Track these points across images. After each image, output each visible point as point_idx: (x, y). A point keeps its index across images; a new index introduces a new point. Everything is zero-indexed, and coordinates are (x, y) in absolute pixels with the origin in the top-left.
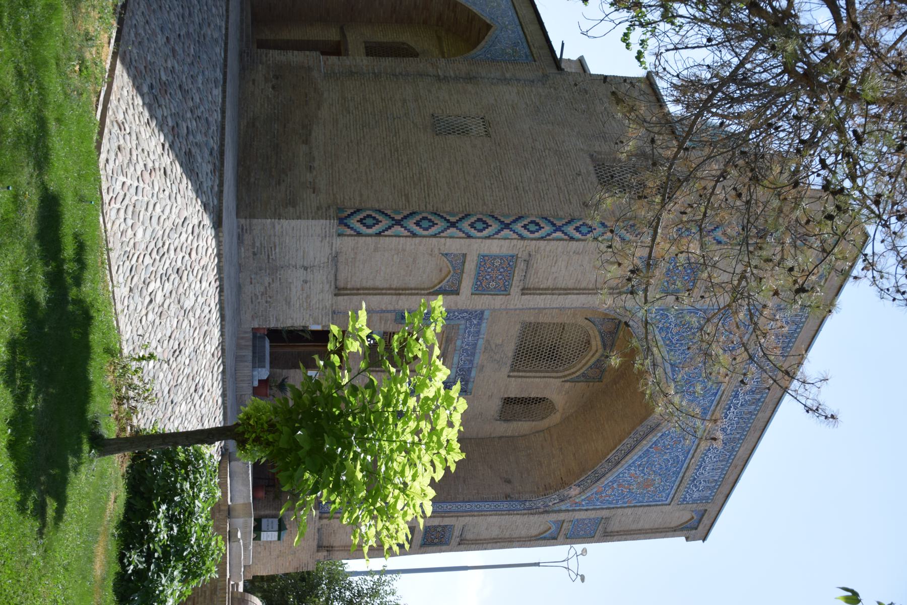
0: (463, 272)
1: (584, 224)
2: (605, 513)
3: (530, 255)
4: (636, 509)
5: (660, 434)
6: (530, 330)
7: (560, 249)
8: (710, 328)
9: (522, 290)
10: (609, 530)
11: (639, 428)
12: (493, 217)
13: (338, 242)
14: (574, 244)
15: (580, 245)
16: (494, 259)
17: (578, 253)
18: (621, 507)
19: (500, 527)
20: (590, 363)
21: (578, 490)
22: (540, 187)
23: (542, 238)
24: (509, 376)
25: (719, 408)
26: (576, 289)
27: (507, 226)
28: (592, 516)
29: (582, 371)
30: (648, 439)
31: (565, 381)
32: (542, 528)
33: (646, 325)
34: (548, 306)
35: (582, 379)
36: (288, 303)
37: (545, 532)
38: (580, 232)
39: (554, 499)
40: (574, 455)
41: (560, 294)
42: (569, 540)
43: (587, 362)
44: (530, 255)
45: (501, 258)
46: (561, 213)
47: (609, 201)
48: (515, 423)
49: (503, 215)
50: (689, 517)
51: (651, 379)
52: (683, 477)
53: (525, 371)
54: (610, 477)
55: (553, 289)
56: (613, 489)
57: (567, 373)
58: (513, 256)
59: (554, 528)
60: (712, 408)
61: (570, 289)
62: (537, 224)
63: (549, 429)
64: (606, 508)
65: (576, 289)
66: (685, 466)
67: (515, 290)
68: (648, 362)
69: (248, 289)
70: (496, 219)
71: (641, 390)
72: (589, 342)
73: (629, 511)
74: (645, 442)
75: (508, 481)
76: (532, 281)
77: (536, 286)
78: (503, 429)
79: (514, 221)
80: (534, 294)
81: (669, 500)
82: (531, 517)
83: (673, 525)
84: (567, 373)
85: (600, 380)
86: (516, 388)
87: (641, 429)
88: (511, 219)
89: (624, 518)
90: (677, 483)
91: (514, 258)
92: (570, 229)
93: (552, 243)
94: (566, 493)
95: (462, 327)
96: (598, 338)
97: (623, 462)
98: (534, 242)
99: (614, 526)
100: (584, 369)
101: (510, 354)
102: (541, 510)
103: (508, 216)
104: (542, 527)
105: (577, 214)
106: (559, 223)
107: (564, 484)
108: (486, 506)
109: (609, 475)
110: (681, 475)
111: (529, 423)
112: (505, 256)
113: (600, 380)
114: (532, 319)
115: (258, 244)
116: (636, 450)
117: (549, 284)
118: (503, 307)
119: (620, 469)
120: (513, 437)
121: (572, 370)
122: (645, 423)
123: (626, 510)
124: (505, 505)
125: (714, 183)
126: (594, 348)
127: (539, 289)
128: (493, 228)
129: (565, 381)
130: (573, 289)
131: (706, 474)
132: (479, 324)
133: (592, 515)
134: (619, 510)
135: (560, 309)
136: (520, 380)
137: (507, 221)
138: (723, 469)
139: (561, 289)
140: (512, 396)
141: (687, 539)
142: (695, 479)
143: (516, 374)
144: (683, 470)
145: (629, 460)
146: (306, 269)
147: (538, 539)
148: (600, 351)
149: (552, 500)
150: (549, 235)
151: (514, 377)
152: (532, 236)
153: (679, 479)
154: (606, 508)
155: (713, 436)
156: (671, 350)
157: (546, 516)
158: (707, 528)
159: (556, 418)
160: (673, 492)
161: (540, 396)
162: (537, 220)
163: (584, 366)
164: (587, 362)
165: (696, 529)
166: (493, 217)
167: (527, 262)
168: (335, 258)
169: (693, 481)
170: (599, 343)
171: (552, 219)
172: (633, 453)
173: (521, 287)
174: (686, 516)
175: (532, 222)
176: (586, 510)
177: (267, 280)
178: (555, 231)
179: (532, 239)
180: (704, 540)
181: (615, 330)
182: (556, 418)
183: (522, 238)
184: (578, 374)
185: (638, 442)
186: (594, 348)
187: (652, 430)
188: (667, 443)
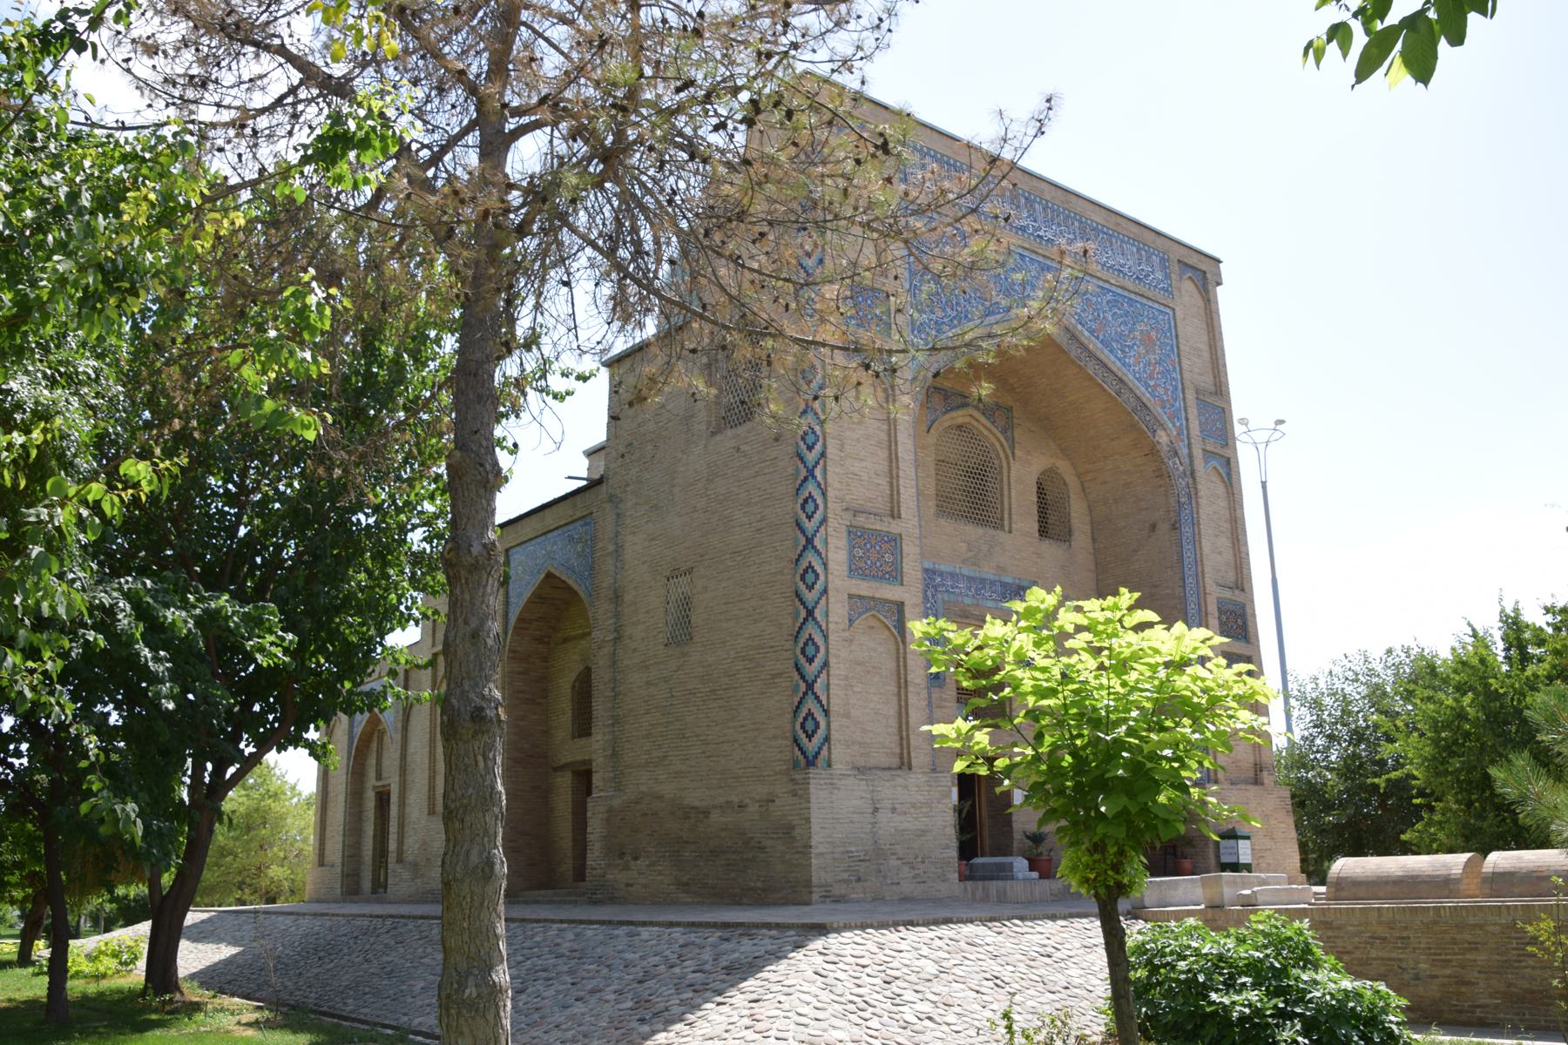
0: (873, 598)
13: (839, 767)
36: (924, 832)
69: (908, 888)
95: (946, 597)
108: (1188, 556)
115: (845, 876)
124: (1187, 530)
132: (941, 574)
146: (876, 810)
159: (1064, 468)
168: (861, 770)
177: (893, 862)
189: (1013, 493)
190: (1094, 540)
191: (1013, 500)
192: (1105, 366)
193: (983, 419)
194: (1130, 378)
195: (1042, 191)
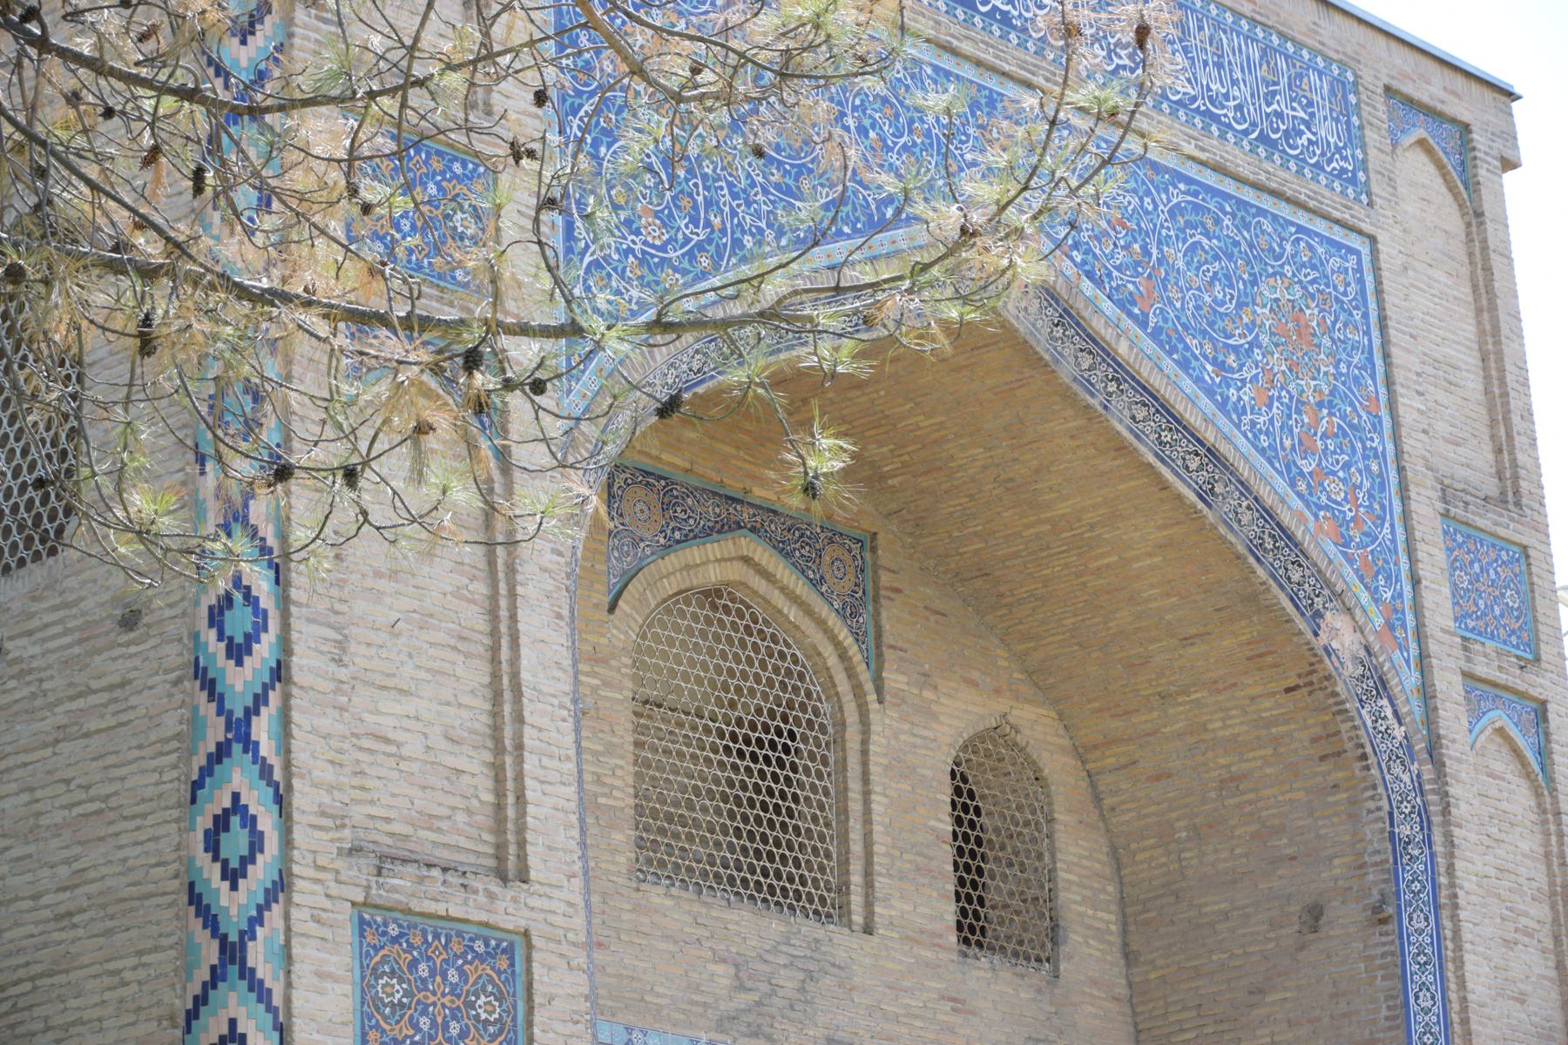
1: (216, 617)
2: (1425, 507)
3: (355, 851)
4: (1399, 375)
5: (1087, 286)
6: (663, 848)
7: (325, 724)
8: (673, 67)
9: (504, 878)
10: (1491, 487)
11: (1066, 373)
12: (192, 1015)
14: (304, 663)
15: (305, 636)
16: (377, 1003)
17: (342, 645)
18: (1396, 438)
19: (1509, 944)
20: (801, 588)
21: (1335, 620)
22: (58, 816)
23: (281, 800)
24: (868, 930)
25: (966, 47)
26: (495, 649)
27: (232, 953)
28: (1441, 557)
29: (833, 621)
30: (1108, 334)
31: (879, 690)
32: (1502, 763)
33: (668, 327)
34: (571, 766)
35: (866, 618)
37: (1516, 752)
38: (251, 639)
39: (1378, 717)
40: (1187, 640)
41: (519, 719)
42: (1546, 652)
44: (355, 851)
45: (369, 974)
46: (172, 723)
47: (140, 502)
48: (1063, 896)
49: (188, 970)
50: (1419, 159)
51: (894, 302)
52: (1257, 187)
53: (844, 863)
54: (1274, 487)
55: (499, 749)
56: (1323, 473)
57: (843, 686)
58: (362, 924)
59: (1499, 717)
60: (968, 72)
61: (496, 676)
62: (221, 822)
63: (1081, 753)
64: (1404, 498)
65: (495, 649)
66: (1210, 178)
67: (507, 910)
68: (825, 316)
70: (201, 1000)
71: (944, 343)
72: (711, 595)
73: (1409, 406)
74: (1123, 348)
75: (1314, 915)
76: (466, 836)
77: (484, 818)
78: (1090, 947)
79: (211, 921)
80: (521, 829)
82: (1460, 811)
83: (1454, 222)
84: (843, 686)
85: (868, 542)
86: (918, 898)
87: (1070, 364)
88: (202, 936)
89: (1438, 427)
90: (1284, 210)
91: (372, 923)
92: (240, 681)
93: (300, 756)
94: (1351, 670)
96: (693, 553)
97: (1210, 436)
98: (298, 835)
99: (1474, 463)
100: (822, 609)
101: (774, 925)
102: (1428, 773)
103: (187, 949)
104: (1498, 767)
105: (175, 655)
106: (215, 731)
107: (1312, 678)
108: (1422, 1002)
109: (1263, 492)
110: (1248, 195)
111: (1061, 837)
112: (363, 956)
113: (868, 542)
114: (623, 837)
116: (1156, 382)
117: (474, 764)
118: (581, 959)
119: (1238, 448)
120: (1122, 901)
121: (832, 660)
122: (1042, 347)
123: (1407, 416)
124: (1417, 923)
125: (54, 64)
126: (735, 572)
127: (499, 807)
128: (241, 1014)
129: (879, 690)
130: (495, 660)
131: (1240, 93)
133: (1433, 558)
134: (1408, 444)
135: (580, 716)
136: (881, 882)
137: (210, 953)
138: (1218, 25)
139: (496, 714)
140: (950, 911)
141: (1509, 164)
142: (1263, 138)
143: (856, 900)
144: (1229, 186)
145: (1197, 409)
147: (1551, 780)
148: (748, 544)
149: (1386, 725)
150: (266, 772)
151: (869, 905)
152: (272, 844)
153: (1267, 203)
154: (1404, 498)
155: (1129, 37)
156: (737, 243)
157: (1450, 751)
158: (1460, 82)
159: (1036, 726)
160: (1320, 226)
161: (946, 796)
162: (204, 822)
163: (808, 611)
165: (1466, 128)
166: (192, 1015)
167: (385, 862)
169: (1273, 144)
170: (713, 549)
171: (200, 760)
172: (1167, 392)
173: (495, 886)
174: (1415, 170)
175: (212, 845)
176: (1416, 582)
178: (250, 746)
179: (287, 843)
180: (1511, 96)
181: (671, 486)
182: (1036, 726)
183: (280, 887)
184: (844, 635)
185: (1122, 374)
186: (735, 572)
187: (1068, 317)
188: (1121, 257)
189: (878, 805)
192: (1165, 409)
193: (784, 572)
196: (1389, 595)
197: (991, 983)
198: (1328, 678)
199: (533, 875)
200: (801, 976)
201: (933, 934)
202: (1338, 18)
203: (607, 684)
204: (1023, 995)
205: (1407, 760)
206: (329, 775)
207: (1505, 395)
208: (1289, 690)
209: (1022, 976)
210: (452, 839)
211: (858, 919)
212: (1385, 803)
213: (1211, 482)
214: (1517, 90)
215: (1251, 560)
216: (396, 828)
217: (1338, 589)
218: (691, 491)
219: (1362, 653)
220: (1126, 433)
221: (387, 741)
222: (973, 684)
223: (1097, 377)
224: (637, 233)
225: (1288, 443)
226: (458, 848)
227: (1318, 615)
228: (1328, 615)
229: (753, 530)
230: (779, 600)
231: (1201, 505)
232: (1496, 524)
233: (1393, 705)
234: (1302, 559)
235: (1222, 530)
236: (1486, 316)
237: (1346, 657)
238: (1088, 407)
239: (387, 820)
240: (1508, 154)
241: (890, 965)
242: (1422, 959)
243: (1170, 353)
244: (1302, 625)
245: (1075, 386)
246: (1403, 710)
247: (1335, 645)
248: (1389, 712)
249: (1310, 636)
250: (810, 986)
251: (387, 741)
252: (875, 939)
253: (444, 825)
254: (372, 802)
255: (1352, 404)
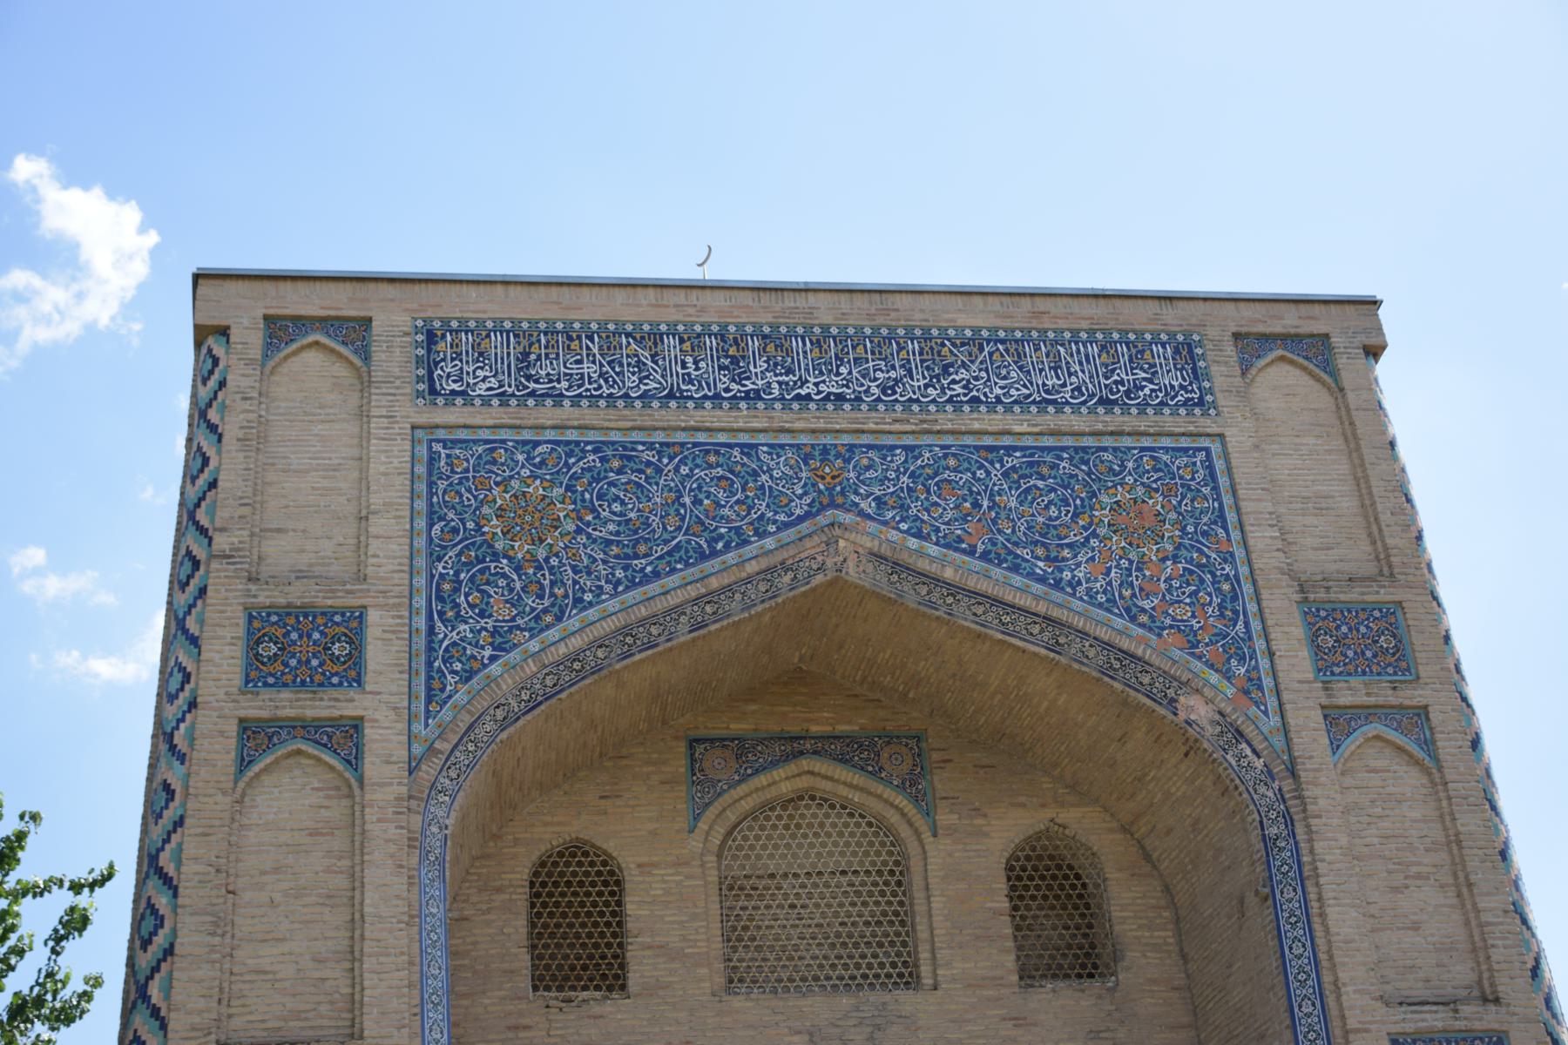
30: (933, 568)
43: (856, 788)
81: (1205, 443)
94: (1210, 730)
96: (763, 779)
100: (888, 793)
104: (1380, 764)
108: (1297, 951)
122: (886, 591)
124: (1288, 896)
126: (804, 783)
143: (925, 969)
148: (805, 763)
159: (1084, 824)
164: (856, 788)
180: (1375, 303)
189: (937, 903)
190: (1184, 957)
191: (937, 919)
192: (997, 601)
193: (841, 772)
194: (1073, 610)
195: (811, 312)
196: (1243, 670)
197: (1061, 1004)
198: (1196, 741)
199: (366, 1033)
200: (870, 1029)
201: (994, 978)
202: (1181, 304)
203: (688, 877)
204: (1083, 1003)
205: (1269, 781)
206: (201, 1003)
207: (1373, 504)
208: (1186, 755)
209: (1083, 991)
210: (319, 1022)
211: (927, 981)
212: (1256, 816)
213: (1055, 637)
214: (1379, 298)
215: (1106, 679)
216: (269, 1025)
217: (1184, 679)
218: (761, 741)
219: (1217, 717)
220: (973, 626)
221: (266, 972)
222: (1023, 805)
223: (935, 597)
224: (490, 616)
225: (1127, 593)
226: (321, 1027)
227: (1173, 701)
228: (1182, 699)
229: (815, 753)
230: (844, 791)
231: (1052, 655)
232: (1363, 594)
233: (1250, 745)
234: (1147, 668)
235: (1076, 666)
236: (1354, 455)
237: (1205, 723)
238: (938, 618)
239: (263, 1021)
240: (1373, 341)
241: (953, 1007)
242: (1293, 920)
243: (999, 565)
244: (1162, 711)
245: (922, 608)
246: (1259, 747)
247: (1193, 717)
248: (1248, 752)
249: (1171, 716)
250: (878, 1035)
251: (266, 972)
252: (939, 992)
253: (310, 1015)
254: (251, 1013)
255: (1200, 551)
